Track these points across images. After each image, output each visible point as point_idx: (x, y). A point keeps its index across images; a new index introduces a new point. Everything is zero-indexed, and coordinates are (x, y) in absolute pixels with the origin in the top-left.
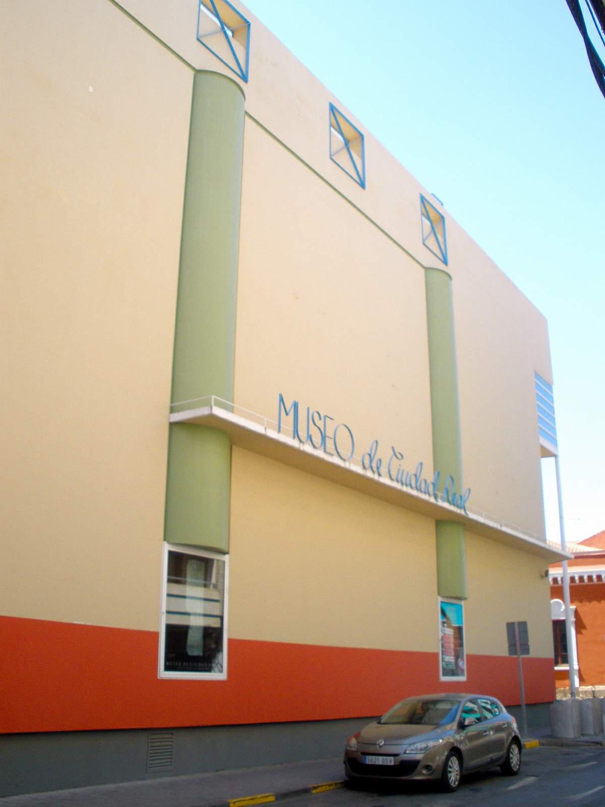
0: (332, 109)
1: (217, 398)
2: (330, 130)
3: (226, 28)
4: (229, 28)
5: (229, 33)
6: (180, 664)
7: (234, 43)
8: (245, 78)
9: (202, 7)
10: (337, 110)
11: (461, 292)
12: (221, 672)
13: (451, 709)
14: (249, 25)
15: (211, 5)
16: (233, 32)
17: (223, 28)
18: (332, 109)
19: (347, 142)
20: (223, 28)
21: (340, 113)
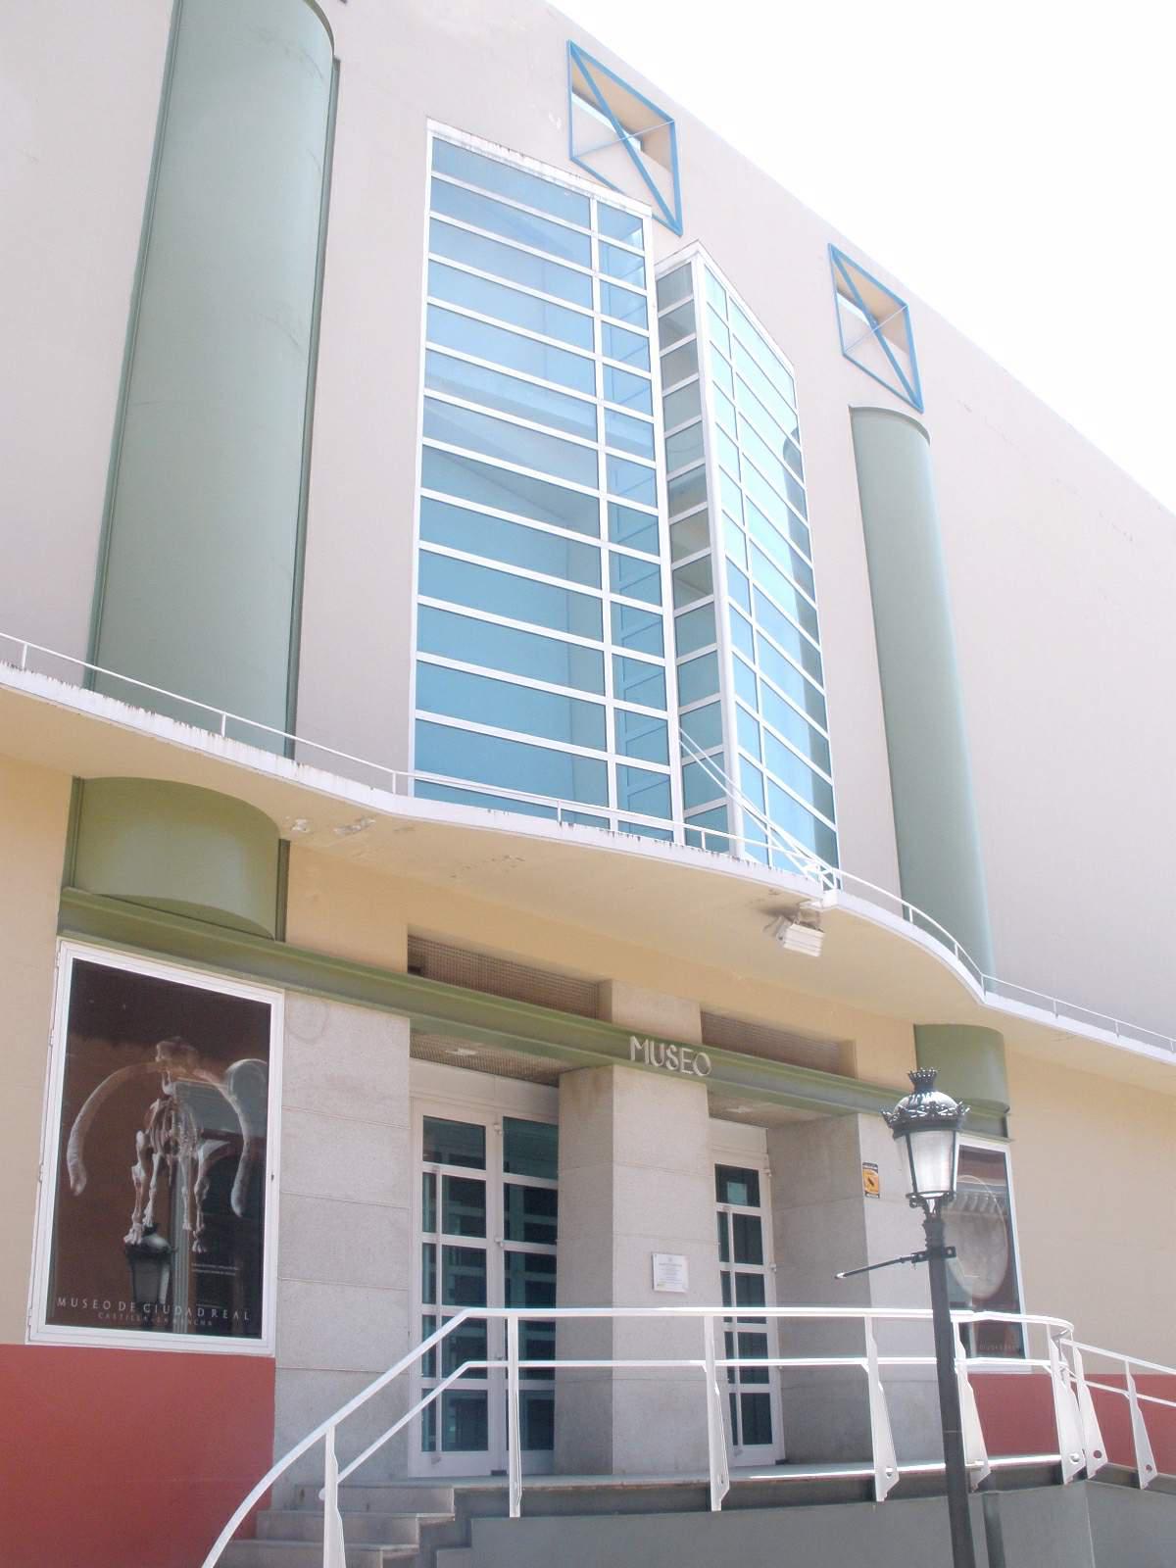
0: (836, 256)
1: (919, 911)
2: (836, 299)
3: (627, 135)
4: (631, 132)
5: (636, 144)
6: (107, 1305)
7: (643, 157)
8: (916, 403)
9: (575, 98)
10: (583, 53)
11: (951, 472)
12: (53, 1319)
13: (1080, 1350)
14: (673, 124)
15: (843, 279)
16: (642, 140)
17: (621, 135)
18: (836, 256)
19: (875, 319)
20: (621, 135)
21: (590, 59)
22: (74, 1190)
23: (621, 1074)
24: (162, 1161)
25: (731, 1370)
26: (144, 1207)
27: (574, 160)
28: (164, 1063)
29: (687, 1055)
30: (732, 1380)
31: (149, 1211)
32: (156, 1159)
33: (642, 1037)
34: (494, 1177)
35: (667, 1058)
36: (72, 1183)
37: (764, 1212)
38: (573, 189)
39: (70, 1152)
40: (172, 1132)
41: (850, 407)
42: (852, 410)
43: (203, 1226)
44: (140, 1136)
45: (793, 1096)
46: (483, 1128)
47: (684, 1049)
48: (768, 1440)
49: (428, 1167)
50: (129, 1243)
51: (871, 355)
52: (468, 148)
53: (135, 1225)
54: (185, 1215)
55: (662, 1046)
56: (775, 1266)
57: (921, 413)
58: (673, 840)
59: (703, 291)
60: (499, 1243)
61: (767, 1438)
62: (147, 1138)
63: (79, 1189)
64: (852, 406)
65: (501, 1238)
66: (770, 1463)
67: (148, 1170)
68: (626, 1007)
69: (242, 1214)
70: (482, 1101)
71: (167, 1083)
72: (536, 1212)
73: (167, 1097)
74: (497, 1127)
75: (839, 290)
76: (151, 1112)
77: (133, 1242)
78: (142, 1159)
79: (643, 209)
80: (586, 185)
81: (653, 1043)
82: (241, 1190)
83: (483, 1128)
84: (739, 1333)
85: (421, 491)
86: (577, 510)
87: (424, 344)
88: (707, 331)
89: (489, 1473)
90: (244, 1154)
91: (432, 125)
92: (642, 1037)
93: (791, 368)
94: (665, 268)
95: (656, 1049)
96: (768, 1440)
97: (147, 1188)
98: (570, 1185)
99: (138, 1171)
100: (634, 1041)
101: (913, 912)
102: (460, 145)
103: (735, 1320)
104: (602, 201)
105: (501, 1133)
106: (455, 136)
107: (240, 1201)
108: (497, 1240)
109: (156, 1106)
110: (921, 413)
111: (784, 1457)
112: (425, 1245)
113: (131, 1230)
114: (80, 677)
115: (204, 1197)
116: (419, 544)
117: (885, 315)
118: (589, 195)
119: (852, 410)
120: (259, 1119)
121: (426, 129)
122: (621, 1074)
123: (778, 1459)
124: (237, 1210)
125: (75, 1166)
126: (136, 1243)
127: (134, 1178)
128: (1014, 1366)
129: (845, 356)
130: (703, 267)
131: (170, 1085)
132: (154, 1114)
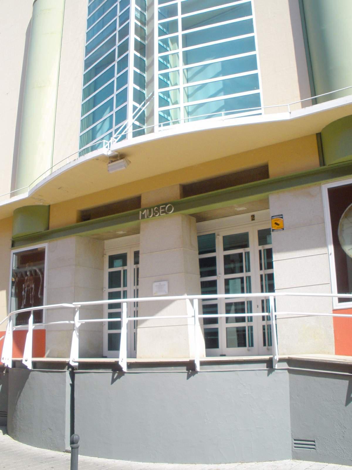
6: (37, 320)
24: (27, 289)
26: (24, 300)
32: (26, 289)
44: (24, 285)
53: (23, 304)
57: (134, 54)
58: (270, 229)
62: (25, 285)
66: (277, 290)
67: (25, 292)
89: (191, 316)
99: (23, 293)
103: (269, 271)
110: (134, 54)
112: (126, 286)
120: (43, 274)
128: (23, 311)
130: (349, 251)
132: (26, 280)
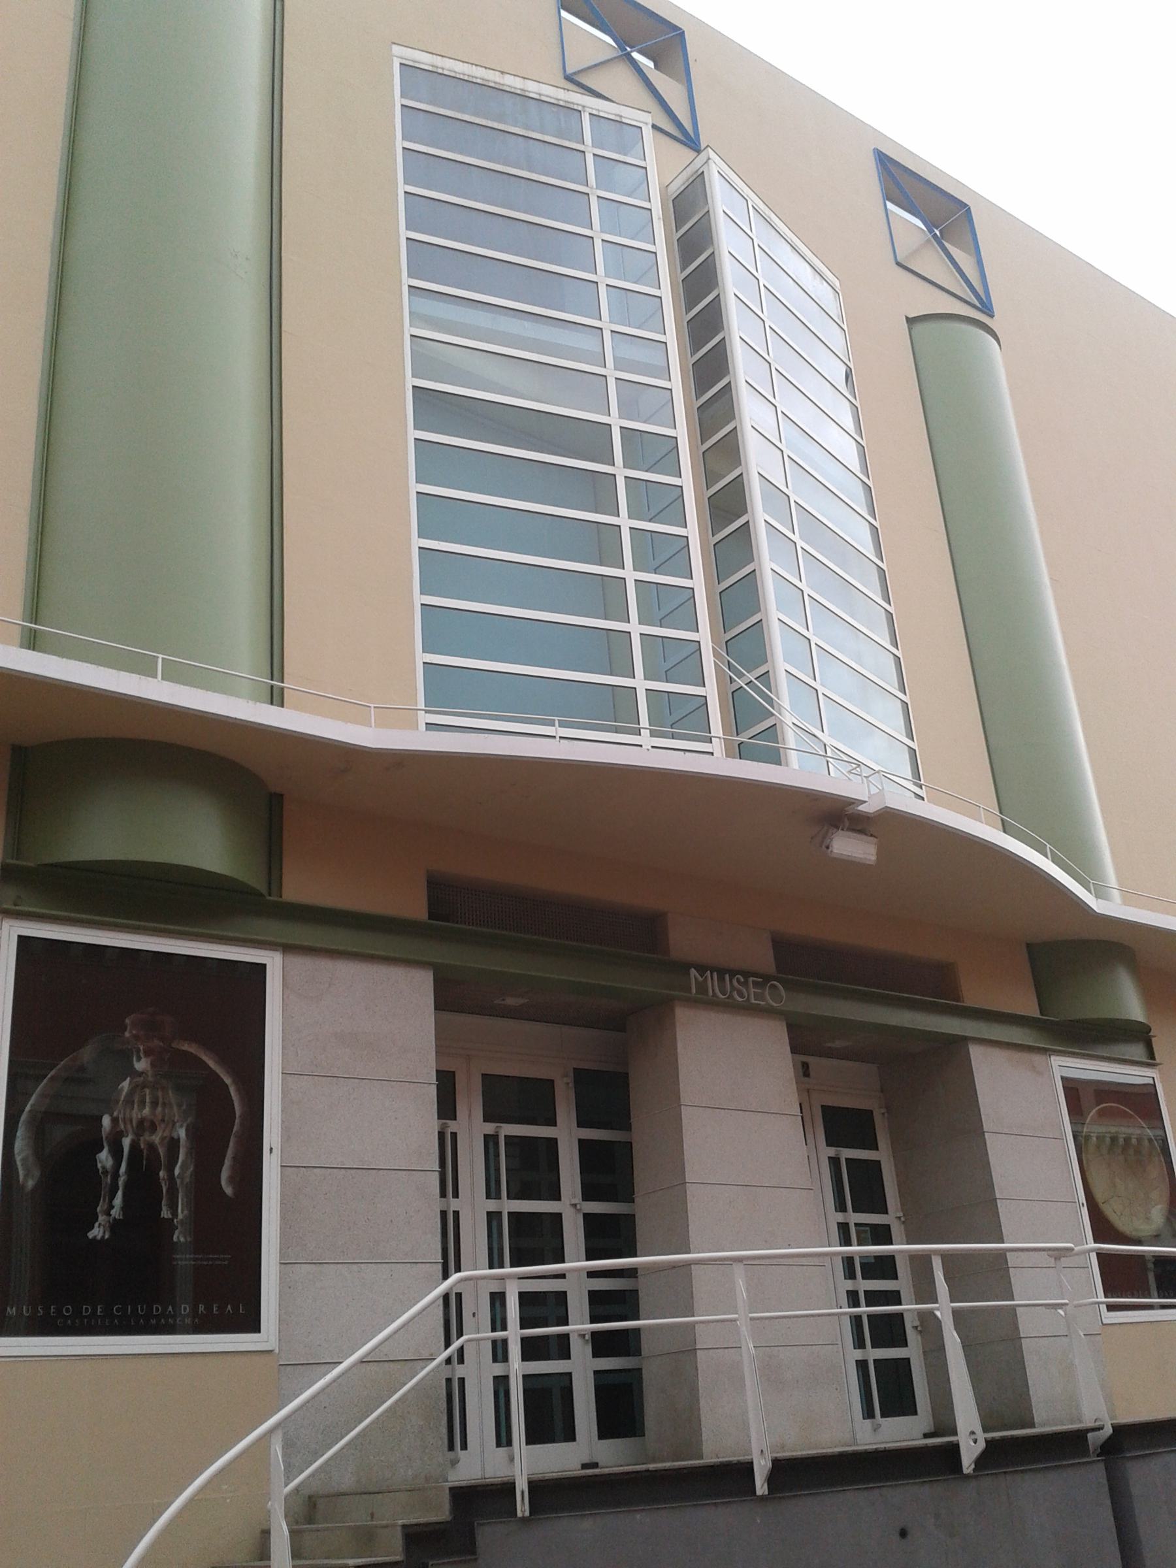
8: (987, 309)
22: (23, 1187)
23: (682, 1014)
24: (134, 1146)
25: (849, 1261)
26: (112, 1196)
27: (569, 78)
28: (136, 1037)
29: (755, 984)
30: (850, 1274)
31: (118, 1201)
32: (126, 1142)
33: (702, 969)
34: (567, 1135)
35: (733, 988)
36: (21, 1178)
37: (883, 1155)
38: (561, 103)
39: (19, 1144)
40: (147, 1111)
41: (907, 318)
42: (910, 321)
43: (186, 1212)
44: (106, 1121)
45: (152, 925)
46: (552, 1081)
47: (751, 979)
48: (914, 1412)
49: (490, 1128)
50: (95, 1238)
51: (932, 265)
52: (440, 71)
54: (164, 1202)
55: (727, 977)
56: (901, 1214)
57: (992, 316)
59: (723, 199)
60: (575, 1205)
61: (909, 1408)
62: (115, 1121)
63: (30, 1184)
64: (911, 316)
65: (578, 1199)
67: (117, 1153)
68: (684, 940)
69: (235, 1194)
70: (538, 1052)
71: (139, 1059)
72: (608, 1171)
73: (141, 1074)
74: (565, 1080)
75: (888, 197)
76: (122, 1089)
77: (99, 1238)
78: (109, 1145)
79: (644, 118)
80: (577, 98)
81: (715, 975)
82: (233, 1168)
83: (552, 1081)
84: (875, 1361)
85: (413, 434)
86: (594, 441)
87: (406, 281)
88: (729, 242)
90: (235, 1128)
91: (396, 50)
92: (702, 969)
93: (837, 284)
94: (676, 188)
95: (728, 988)
96: (914, 1412)
97: (116, 1175)
98: (643, 1135)
99: (104, 1158)
100: (693, 971)
101: (291, 1471)
102: (430, 68)
104: (594, 112)
105: (571, 1085)
106: (425, 60)
107: (231, 1180)
108: (573, 1202)
109: (126, 1085)
110: (992, 316)
111: (933, 1430)
113: (97, 1225)
114: (16, 633)
115: (187, 1180)
116: (415, 487)
117: (944, 213)
118: (580, 108)
119: (910, 321)
121: (391, 56)
122: (682, 1014)
123: (927, 1431)
124: (229, 1191)
125: (24, 1160)
126: (103, 1237)
127: (99, 1165)
129: (898, 264)
131: (143, 1060)
